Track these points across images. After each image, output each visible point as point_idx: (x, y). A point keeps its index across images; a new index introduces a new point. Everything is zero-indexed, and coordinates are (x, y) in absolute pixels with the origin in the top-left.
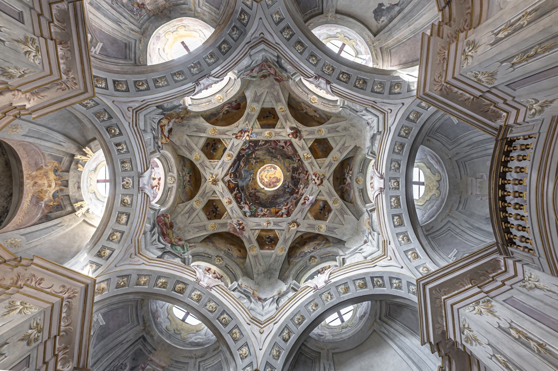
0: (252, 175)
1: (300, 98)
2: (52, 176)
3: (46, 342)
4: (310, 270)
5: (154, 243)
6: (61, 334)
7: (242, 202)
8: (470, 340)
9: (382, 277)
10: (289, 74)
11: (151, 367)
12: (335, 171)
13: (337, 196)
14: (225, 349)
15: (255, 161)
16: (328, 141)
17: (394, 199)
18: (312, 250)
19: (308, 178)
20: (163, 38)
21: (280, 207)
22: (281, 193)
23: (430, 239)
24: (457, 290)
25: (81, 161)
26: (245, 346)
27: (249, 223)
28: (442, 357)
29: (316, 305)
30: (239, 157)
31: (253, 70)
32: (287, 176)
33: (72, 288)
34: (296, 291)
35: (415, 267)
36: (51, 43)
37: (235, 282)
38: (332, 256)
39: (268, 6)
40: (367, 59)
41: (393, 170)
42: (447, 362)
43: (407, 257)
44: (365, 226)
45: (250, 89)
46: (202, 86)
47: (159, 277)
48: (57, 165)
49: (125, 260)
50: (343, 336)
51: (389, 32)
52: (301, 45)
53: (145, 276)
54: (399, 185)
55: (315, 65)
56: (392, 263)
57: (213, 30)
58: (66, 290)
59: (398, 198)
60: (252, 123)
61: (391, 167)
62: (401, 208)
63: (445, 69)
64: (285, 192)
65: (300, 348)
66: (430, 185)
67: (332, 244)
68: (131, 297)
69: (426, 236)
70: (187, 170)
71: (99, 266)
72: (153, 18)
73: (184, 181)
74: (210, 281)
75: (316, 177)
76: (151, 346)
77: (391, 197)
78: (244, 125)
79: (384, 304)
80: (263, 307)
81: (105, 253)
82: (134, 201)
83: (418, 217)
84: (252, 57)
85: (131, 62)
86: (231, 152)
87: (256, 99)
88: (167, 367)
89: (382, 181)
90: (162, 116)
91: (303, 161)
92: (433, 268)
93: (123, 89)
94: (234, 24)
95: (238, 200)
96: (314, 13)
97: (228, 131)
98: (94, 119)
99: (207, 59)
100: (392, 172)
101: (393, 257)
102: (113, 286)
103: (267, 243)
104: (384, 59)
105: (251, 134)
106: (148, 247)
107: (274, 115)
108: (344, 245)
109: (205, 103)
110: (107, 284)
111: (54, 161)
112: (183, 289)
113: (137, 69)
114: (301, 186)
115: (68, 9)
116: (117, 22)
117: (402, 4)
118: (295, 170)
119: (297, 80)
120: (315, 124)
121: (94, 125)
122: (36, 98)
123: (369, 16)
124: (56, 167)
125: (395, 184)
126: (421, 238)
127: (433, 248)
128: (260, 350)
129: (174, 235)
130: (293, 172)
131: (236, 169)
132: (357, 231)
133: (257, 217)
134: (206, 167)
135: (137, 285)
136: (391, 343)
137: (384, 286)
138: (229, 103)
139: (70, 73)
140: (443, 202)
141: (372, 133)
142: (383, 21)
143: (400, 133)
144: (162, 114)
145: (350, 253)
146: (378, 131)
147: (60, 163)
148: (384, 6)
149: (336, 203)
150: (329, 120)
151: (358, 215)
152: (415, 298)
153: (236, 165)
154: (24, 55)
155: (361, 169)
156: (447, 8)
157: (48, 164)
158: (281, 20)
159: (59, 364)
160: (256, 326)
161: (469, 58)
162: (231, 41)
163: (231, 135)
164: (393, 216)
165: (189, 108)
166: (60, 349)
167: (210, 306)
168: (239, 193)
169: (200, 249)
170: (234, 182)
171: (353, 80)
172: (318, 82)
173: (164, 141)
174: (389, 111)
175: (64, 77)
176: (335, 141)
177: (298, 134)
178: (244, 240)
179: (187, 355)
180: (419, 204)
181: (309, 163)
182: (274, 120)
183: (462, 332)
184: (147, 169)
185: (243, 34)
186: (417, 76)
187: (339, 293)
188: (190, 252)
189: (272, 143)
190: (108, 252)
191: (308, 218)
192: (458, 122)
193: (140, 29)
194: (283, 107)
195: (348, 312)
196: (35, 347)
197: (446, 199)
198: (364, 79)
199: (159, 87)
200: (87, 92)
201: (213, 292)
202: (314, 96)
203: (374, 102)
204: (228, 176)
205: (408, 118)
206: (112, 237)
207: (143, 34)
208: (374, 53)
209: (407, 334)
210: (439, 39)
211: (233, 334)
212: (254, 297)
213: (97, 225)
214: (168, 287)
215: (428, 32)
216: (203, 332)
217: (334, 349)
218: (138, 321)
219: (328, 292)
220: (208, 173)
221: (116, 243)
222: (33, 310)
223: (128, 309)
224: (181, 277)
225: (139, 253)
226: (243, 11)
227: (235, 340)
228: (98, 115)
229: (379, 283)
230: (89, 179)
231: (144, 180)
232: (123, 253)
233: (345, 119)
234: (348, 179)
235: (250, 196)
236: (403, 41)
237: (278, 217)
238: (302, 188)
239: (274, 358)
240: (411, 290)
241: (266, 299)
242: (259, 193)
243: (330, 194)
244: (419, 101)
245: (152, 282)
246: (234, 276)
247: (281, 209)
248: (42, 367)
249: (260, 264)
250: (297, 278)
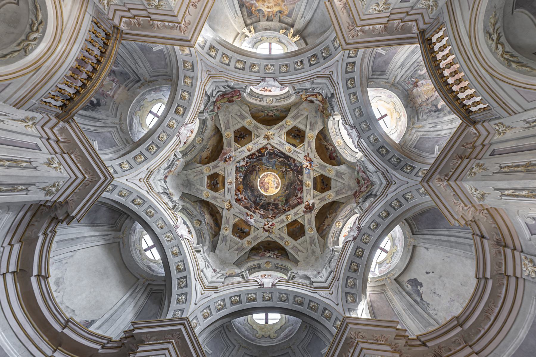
0: (271, 168)
1: (340, 212)
2: (276, 9)
3: (147, 10)
4: (189, 220)
5: (217, 88)
7: (248, 160)
10: (361, 204)
11: (115, 87)
12: (276, 242)
13: (254, 244)
14: (128, 149)
15: (284, 170)
16: (302, 237)
17: (254, 296)
18: (207, 222)
19: (269, 218)
20: (389, 100)
21: (243, 193)
22: (256, 194)
23: (220, 329)
24: (180, 353)
25: (288, 32)
26: (130, 166)
27: (231, 167)
28: (120, 341)
29: (162, 228)
30: (287, 157)
31: (364, 173)
32: (271, 199)
33: (188, 30)
34: (173, 208)
35: (196, 316)
36: (385, 20)
37: (181, 155)
38: (202, 241)
39: (418, 189)
40: (375, 272)
41: (280, 296)
42: (116, 345)
43: (205, 309)
44: (229, 270)
45: (347, 169)
46: (350, 131)
47: (190, 94)
48: (285, 13)
49: (205, 67)
50: (134, 251)
51: (398, 292)
52: (386, 216)
53: (192, 83)
54: (266, 301)
55: (369, 227)
56: (199, 295)
57: (397, 142)
58: (187, 25)
59: (255, 300)
60: (317, 170)
61: (282, 293)
62: (247, 303)
63: (369, 341)
64: (256, 197)
65: (125, 213)
66: (265, 329)
67: (211, 240)
68: (175, 71)
69: (222, 326)
70: (278, 113)
71: (203, 47)
72: (406, 93)
73: (268, 111)
74: (184, 135)
75: (271, 225)
76: (132, 87)
77: (256, 294)
78: (316, 163)
79: (163, 288)
80: (159, 180)
82: (254, 74)
83: (238, 319)
84: (375, 174)
85: (370, 75)
86: (292, 151)
87: (339, 174)
88: (113, 100)
89: (270, 286)
90: (324, 96)
91: (285, 214)
92: (197, 331)
93: (348, 69)
94: (402, 160)
95: (250, 157)
96: (413, 227)
97: (311, 149)
98: (324, 46)
100: (278, 294)
101: (204, 296)
102: (185, 58)
103: (213, 182)
104: (375, 288)
105: (308, 169)
106: (215, 84)
107: (325, 189)
108: (212, 251)
109: (335, 131)
110: (187, 54)
111: (288, 11)
112: (179, 113)
113: (364, 80)
114: (262, 212)
115: (412, 33)
116: (402, 66)
117: (423, 304)
118: (276, 206)
119: (356, 211)
120: (318, 225)
121: (318, 45)
122: (342, 6)
123: (412, 275)
124: (284, 12)
125: (267, 297)
126: (221, 321)
127: (212, 332)
128: (127, 180)
129: (222, 103)
130: (274, 204)
131: (277, 155)
132: (223, 263)
133: (236, 173)
134: (280, 130)
135: (184, 76)
136: (128, 294)
137: (179, 288)
138: (335, 150)
139: (361, 33)
140: (252, 340)
141: (311, 276)
142: (407, 286)
143: (312, 301)
144: (327, 97)
145: (205, 257)
146: (313, 282)
147: (287, 16)
148: (420, 288)
149: (248, 243)
150: (321, 237)
151: (238, 263)
152: (169, 316)
153: (280, 155)
154: (376, 2)
155: (279, 266)
156: (419, 343)
157: (286, 7)
158: (407, 200)
159: (127, 19)
160: (145, 175)
162: (389, 157)
163: (308, 152)
164: (239, 296)
165: (331, 118)
166: (139, 20)
167: (164, 136)
168: (257, 157)
169: (210, 125)
170: (266, 153)
171: (357, 260)
172: (354, 230)
173: (303, 96)
174: (331, 292)
175: (359, 29)
176: (303, 243)
177: (308, 210)
178: (216, 162)
179: (123, 116)
180: (249, 319)
181: (283, 219)
182: (321, 189)
184: (281, 84)
185: (395, 167)
186: (362, 317)
187: (172, 248)
188: (208, 117)
189: (300, 187)
190: (213, 54)
191: (234, 219)
192: (323, 353)
193: (397, 83)
194: (332, 197)
195: (155, 255)
196: (143, 3)
197: (254, 343)
198: (358, 270)
199: (350, 97)
200: (346, 45)
201: (175, 138)
202: (342, 225)
203: (339, 279)
204: (271, 148)
205: (325, 309)
207: (393, 85)
208: (380, 278)
209: (136, 309)
210: (394, 337)
211: (140, 156)
212: (168, 172)
213: (234, 44)
214: (182, 101)
215: (399, 327)
216: (140, 129)
217: (123, 243)
218: (154, 76)
219: (173, 238)
220: (275, 131)
221: (220, 59)
222: (173, 2)
223: (165, 69)
224: (189, 111)
225: (210, 77)
226: (413, 168)
227: (135, 158)
228: (327, 48)
229: (181, 283)
230: (273, 37)
231: (271, 82)
232: (212, 65)
233: (322, 252)
234: (269, 255)
235: (253, 166)
236: (391, 305)
237: (235, 191)
238: (260, 212)
239: (119, 192)
241: (166, 182)
242: (255, 174)
243: (255, 238)
244: (341, 319)
245: (186, 88)
246: (186, 154)
247: (241, 194)
248: (126, 7)
249: (195, 176)
250: (184, 210)
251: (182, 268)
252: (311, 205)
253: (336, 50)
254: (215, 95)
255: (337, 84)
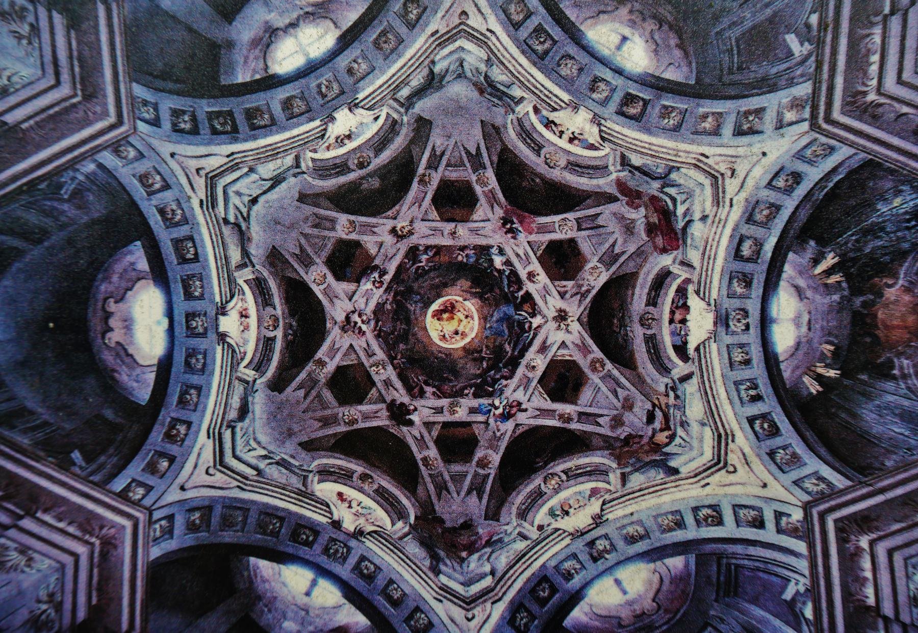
5: (684, 197)
6: (879, 18)
7: (507, 273)
8: (16, 12)
9: (215, 132)
19: (377, 323)
21: (430, 264)
30: (514, 363)
41: (200, 353)
47: (677, 128)
56: (193, 164)
59: (189, 296)
61: (205, 358)
62: (181, 277)
81: (787, 180)
90: (667, 450)
99: (578, 566)
105: (490, 410)
125: (194, 324)
146: (233, 428)
161: (45, 598)
168: (513, 293)
170: (523, 313)
172: (357, 523)
173: (663, 400)
183: (35, 29)
187: (303, 98)
201: (566, 97)
204: (534, 326)
205: (172, 460)
206: (771, 213)
229: (221, 120)
237: (435, 246)
240: (152, 110)
245: (690, 121)
247: (428, 260)
251: (258, 122)
252: (408, 417)
253: (796, 483)
254: (666, 194)
255: (703, 482)
